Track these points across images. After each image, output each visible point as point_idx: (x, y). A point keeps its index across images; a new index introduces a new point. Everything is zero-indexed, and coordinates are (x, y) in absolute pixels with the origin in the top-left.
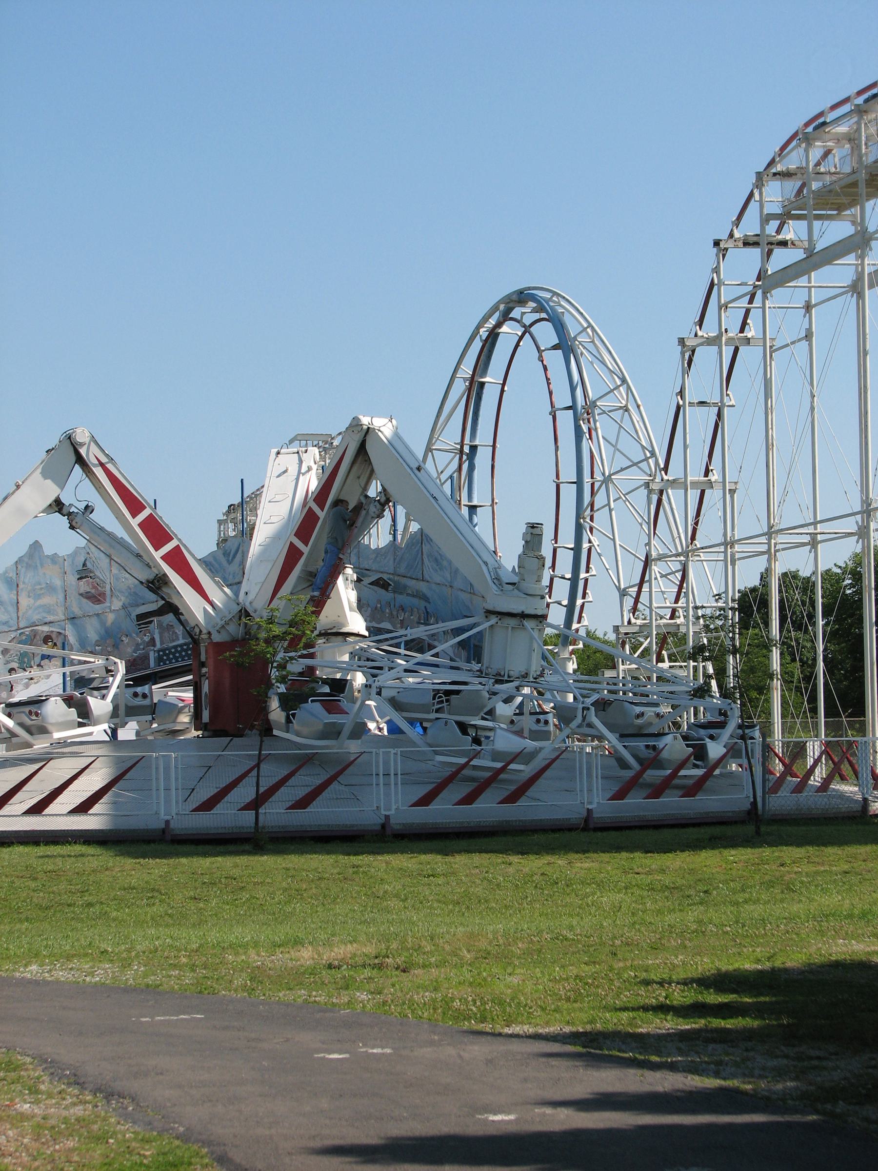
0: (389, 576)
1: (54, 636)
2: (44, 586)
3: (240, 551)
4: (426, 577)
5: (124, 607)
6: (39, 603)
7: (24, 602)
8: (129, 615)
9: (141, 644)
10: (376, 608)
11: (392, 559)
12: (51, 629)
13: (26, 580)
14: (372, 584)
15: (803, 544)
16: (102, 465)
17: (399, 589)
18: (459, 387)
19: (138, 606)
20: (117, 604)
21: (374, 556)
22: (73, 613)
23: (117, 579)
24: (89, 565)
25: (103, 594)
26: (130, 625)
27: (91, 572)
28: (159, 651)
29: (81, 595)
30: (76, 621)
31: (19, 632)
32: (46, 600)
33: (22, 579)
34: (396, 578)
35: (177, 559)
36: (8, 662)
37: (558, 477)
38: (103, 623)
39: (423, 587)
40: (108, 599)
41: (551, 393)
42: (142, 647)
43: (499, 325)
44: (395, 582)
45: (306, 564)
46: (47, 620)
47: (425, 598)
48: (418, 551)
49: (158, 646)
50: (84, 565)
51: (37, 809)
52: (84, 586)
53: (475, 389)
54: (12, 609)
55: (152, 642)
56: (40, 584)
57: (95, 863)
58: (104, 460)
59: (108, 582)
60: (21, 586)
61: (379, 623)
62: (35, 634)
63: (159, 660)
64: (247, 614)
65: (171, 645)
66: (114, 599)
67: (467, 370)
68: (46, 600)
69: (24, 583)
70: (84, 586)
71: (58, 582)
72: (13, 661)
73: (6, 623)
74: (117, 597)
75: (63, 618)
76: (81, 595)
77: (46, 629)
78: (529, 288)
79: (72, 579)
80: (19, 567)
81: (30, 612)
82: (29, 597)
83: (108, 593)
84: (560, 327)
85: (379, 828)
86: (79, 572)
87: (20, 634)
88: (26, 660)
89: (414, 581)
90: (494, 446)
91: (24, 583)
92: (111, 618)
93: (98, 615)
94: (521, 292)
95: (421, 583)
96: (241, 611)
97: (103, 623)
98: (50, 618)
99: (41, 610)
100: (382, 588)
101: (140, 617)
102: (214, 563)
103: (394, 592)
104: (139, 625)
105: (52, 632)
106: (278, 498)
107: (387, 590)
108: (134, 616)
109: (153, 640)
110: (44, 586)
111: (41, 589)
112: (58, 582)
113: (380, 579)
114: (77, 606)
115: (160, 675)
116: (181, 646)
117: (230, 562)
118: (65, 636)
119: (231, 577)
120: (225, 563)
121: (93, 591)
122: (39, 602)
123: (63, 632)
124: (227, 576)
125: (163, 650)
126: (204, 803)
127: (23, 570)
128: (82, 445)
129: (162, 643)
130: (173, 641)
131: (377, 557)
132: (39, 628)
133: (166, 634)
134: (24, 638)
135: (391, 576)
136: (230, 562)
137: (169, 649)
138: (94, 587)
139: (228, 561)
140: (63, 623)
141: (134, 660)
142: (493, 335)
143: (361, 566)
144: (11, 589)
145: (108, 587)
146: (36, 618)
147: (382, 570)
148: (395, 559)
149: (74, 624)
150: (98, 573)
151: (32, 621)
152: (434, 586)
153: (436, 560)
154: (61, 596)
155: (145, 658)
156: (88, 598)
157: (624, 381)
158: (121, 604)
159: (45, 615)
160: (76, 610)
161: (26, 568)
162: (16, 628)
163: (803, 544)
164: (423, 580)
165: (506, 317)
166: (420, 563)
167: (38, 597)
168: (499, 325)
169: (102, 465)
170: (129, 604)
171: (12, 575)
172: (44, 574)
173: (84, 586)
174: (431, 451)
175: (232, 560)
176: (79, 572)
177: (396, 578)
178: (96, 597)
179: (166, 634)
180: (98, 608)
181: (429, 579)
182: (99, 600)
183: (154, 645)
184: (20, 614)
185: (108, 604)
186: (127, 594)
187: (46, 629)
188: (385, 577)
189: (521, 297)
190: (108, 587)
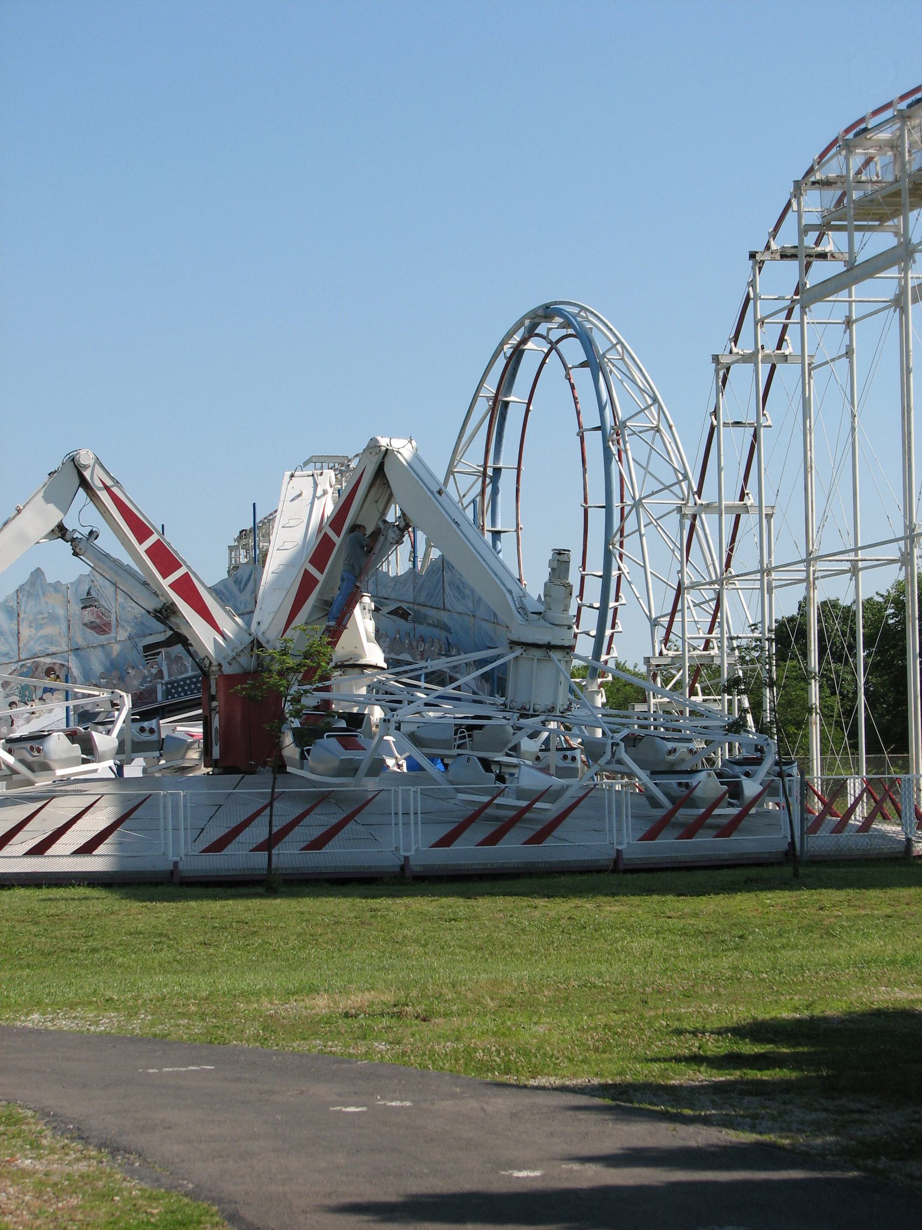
0: (408, 605)
1: (56, 668)
2: (46, 615)
3: (252, 579)
4: (448, 606)
5: (130, 638)
6: (41, 633)
7: (26, 632)
8: (136, 646)
9: (148, 677)
10: (395, 639)
11: (412, 588)
12: (54, 661)
13: (28, 610)
14: (390, 613)
15: (844, 572)
16: (107, 488)
17: (419, 619)
18: (482, 406)
19: (145, 636)
20: (123, 635)
21: (392, 584)
22: (77, 643)
23: (123, 608)
24: (93, 593)
25: (108, 624)
26: (136, 656)
27: (95, 601)
28: (167, 684)
29: (85, 625)
30: (79, 652)
31: (20, 663)
32: (49, 631)
33: (23, 608)
34: (416, 607)
35: (186, 587)
36: (8, 696)
37: (585, 501)
38: (108, 654)
39: (444, 616)
40: (113, 630)
41: (578, 413)
42: (149, 679)
43: (524, 341)
44: (414, 611)
45: (321, 593)
46: (49, 651)
47: (447, 628)
48: (439, 579)
49: (166, 678)
50: (89, 593)
51: (39, 850)
52: (88, 616)
53: (499, 408)
54: (13, 640)
55: (160, 674)
56: (42, 614)
57: (99, 907)
58: (109, 483)
59: (113, 611)
60: (22, 616)
61: (398, 655)
62: (37, 666)
63: (167, 693)
64: (260, 645)
65: (180, 677)
66: (120, 629)
67: (490, 388)
68: (49, 631)
69: (25, 612)
70: (88, 616)
71: (61, 612)
72: (13, 694)
73: (6, 655)
74: (123, 627)
75: (66, 649)
76: (85, 625)
77: (48, 660)
78: (556, 303)
79: (76, 608)
80: (20, 596)
81: (32, 643)
82: (31, 627)
83: (114, 623)
84: (588, 343)
86: (83, 600)
87: (21, 666)
88: (27, 693)
89: (435, 611)
90: (519, 469)
91: (25, 612)
92: (116, 649)
93: (103, 646)
94: (547, 307)
95: (442, 612)
96: (253, 642)
97: (108, 654)
98: (53, 649)
99: (43, 641)
100: (401, 617)
101: (147, 648)
102: (225, 591)
103: (414, 622)
104: (146, 656)
105: (55, 663)
106: (292, 523)
107: (406, 620)
108: (140, 647)
109: (160, 672)
110: (46, 615)
111: (43, 618)
112: (61, 612)
113: (399, 608)
114: (81, 637)
115: (168, 709)
116: (190, 678)
117: (241, 591)
118: (68, 668)
119: (243, 606)
120: (236, 592)
121: (98, 621)
122: (41, 633)
123: (66, 663)
124: (238, 605)
125: (172, 683)
127: (24, 599)
128: (86, 467)
129: (170, 675)
130: (182, 673)
131: (395, 585)
132: (41, 659)
133: (174, 666)
134: (25, 670)
135: (411, 606)
136: (241, 591)
137: (177, 682)
138: (99, 617)
139: (239, 589)
140: (66, 655)
141: (141, 693)
142: (518, 352)
143: (380, 595)
144: (11, 619)
145: (113, 617)
146: (37, 649)
147: (401, 598)
148: (414, 588)
149: (77, 656)
150: (103, 602)
151: (34, 652)
152: (456, 616)
153: (458, 588)
154: (64, 627)
155: (152, 691)
156: (93, 628)
157: (655, 400)
158: (127, 634)
159: (47, 646)
160: (80, 641)
161: (28, 596)
162: (17, 659)
163: (844, 572)
164: (444, 610)
165: (531, 333)
166: (441, 591)
167: (40, 627)
168: (524, 341)
169: (107, 488)
170: (136, 634)
171: (13, 603)
172: (47, 603)
173: (88, 616)
174: (453, 473)
175: (244, 588)
176: (83, 600)
177: (416, 607)
178: (101, 628)
179: (174, 666)
180: (103, 639)
181: (450, 608)
182: (104, 630)
183: (162, 678)
184: (21, 645)
185: (113, 635)
186: (133, 624)
187: (48, 660)
188: (404, 606)
189: (547, 312)
190: (113, 617)
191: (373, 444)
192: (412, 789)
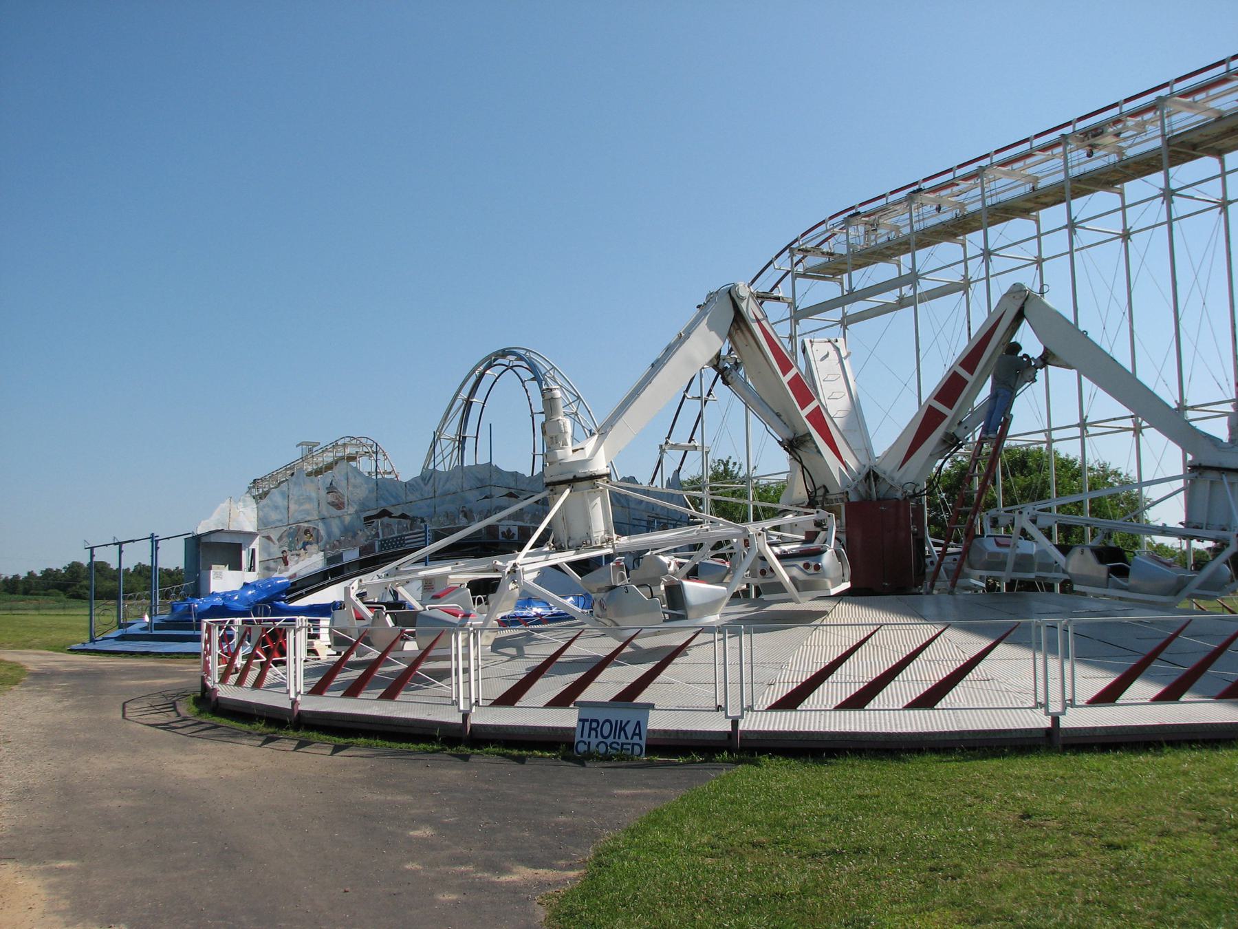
5: (356, 512)
7: (293, 507)
16: (758, 321)
18: (459, 402)
20: (352, 510)
26: (360, 523)
32: (307, 506)
35: (818, 418)
38: (342, 522)
43: (485, 370)
45: (949, 427)
51: (858, 701)
52: (331, 498)
53: (468, 404)
55: (377, 535)
58: (760, 316)
62: (299, 528)
63: (382, 546)
64: (876, 477)
67: (464, 395)
68: (307, 506)
70: (331, 498)
71: (314, 495)
77: (306, 525)
79: (323, 493)
84: (533, 368)
85: (1043, 734)
92: (347, 519)
94: (503, 350)
96: (868, 474)
97: (342, 522)
101: (366, 519)
106: (830, 378)
109: (377, 534)
112: (314, 495)
114: (327, 511)
126: (922, 696)
128: (742, 299)
146: (300, 518)
155: (372, 546)
157: (579, 397)
160: (326, 514)
165: (489, 367)
167: (301, 504)
168: (485, 370)
169: (758, 321)
178: (338, 505)
180: (339, 512)
187: (306, 525)
189: (504, 353)
191: (1017, 289)
192: (1061, 621)
